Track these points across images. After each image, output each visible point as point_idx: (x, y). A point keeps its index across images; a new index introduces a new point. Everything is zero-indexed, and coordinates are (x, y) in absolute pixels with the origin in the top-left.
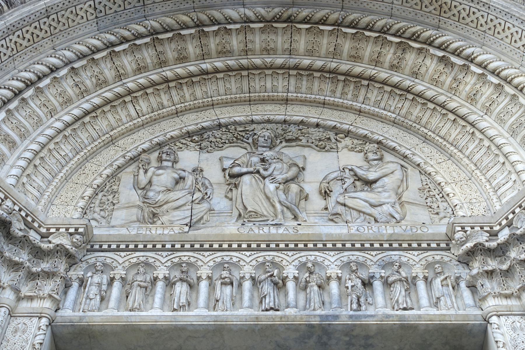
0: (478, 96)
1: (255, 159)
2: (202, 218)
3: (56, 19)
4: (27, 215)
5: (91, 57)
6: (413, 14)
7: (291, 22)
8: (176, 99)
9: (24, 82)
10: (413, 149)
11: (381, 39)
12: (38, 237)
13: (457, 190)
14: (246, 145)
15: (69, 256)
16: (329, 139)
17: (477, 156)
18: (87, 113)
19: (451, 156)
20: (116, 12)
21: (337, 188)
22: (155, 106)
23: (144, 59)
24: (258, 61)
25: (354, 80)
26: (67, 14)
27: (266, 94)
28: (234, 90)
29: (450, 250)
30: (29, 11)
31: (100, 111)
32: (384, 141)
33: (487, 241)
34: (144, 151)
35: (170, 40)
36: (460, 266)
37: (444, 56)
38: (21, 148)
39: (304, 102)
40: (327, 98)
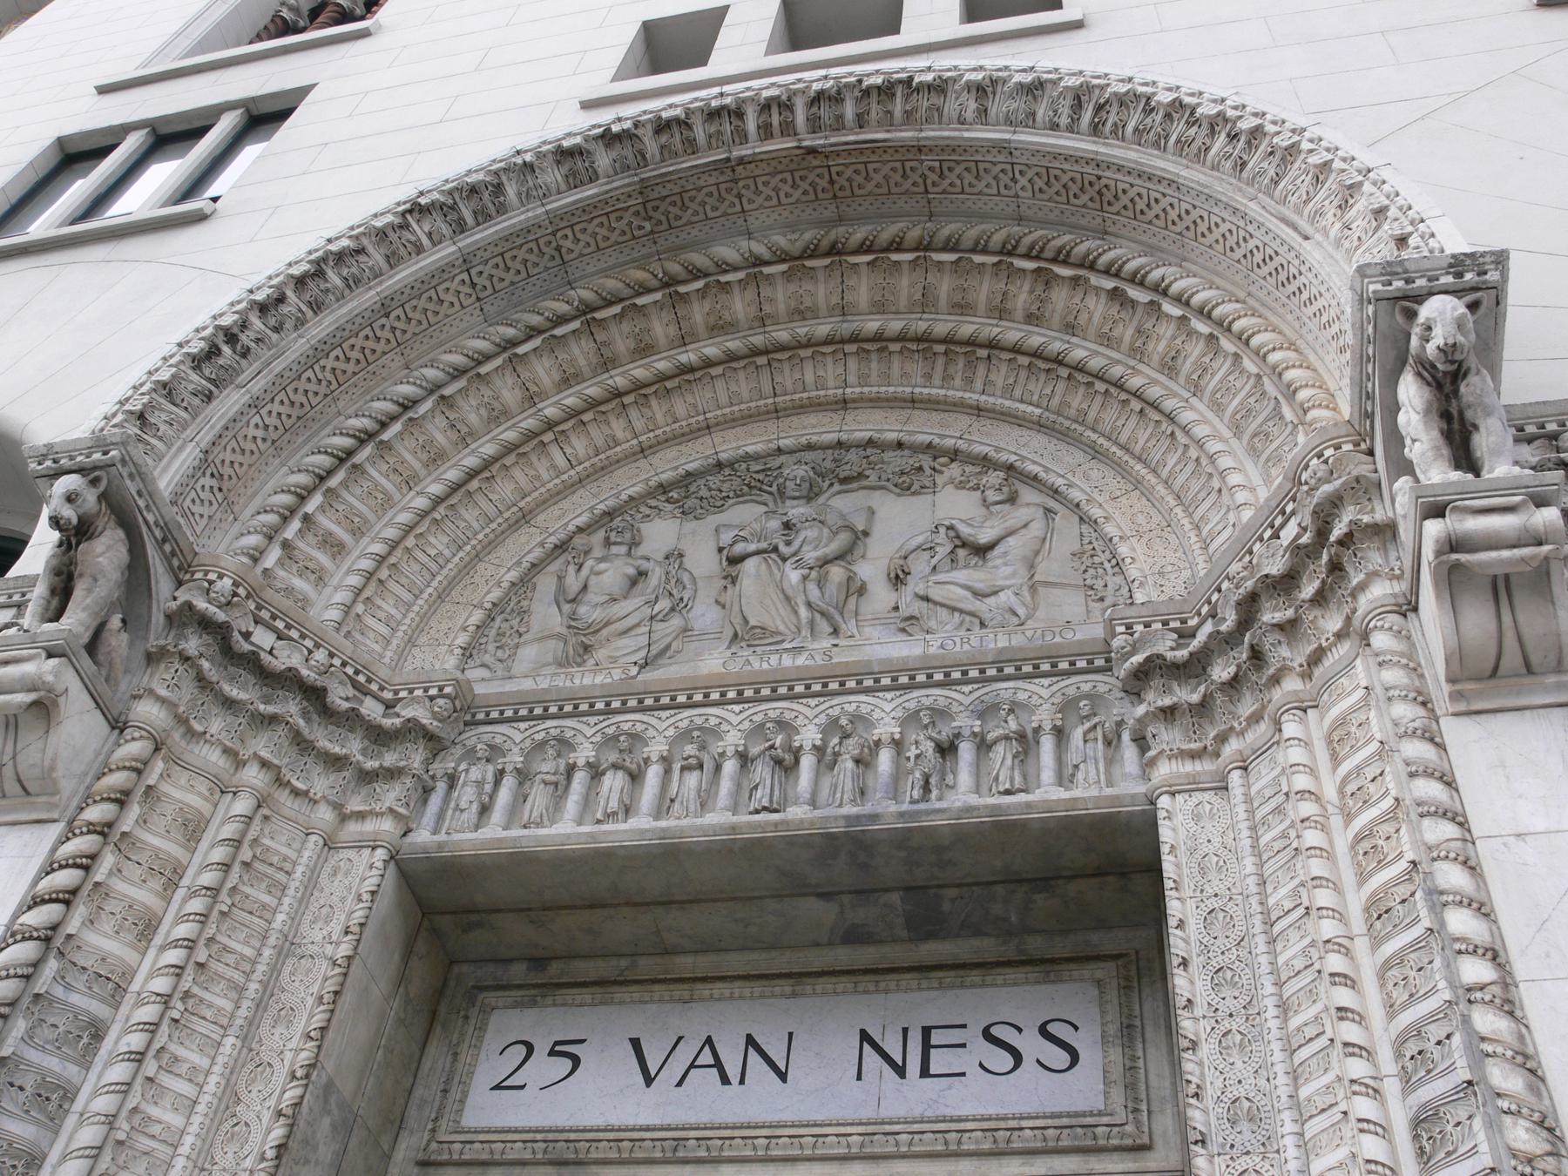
0: (1180, 361)
1: (774, 524)
2: (668, 647)
3: (403, 316)
4: (357, 672)
5: (473, 372)
6: (1057, 212)
7: (839, 253)
8: (639, 425)
9: (354, 436)
10: (1069, 476)
11: (1004, 266)
12: (380, 709)
13: (1139, 551)
14: (766, 496)
15: (429, 736)
16: (920, 469)
17: (1181, 480)
18: (472, 474)
19: (1138, 483)
20: (513, 283)
21: (920, 565)
22: (600, 443)
23: (573, 360)
24: (782, 335)
25: (963, 350)
26: (422, 303)
27: (805, 395)
28: (745, 395)
29: (1110, 669)
30: (351, 311)
31: (497, 465)
32: (1018, 464)
33: (1172, 649)
34: (580, 530)
35: (619, 317)
36: (1127, 702)
37: (1116, 289)
38: (356, 553)
39: (877, 402)
40: (917, 390)
